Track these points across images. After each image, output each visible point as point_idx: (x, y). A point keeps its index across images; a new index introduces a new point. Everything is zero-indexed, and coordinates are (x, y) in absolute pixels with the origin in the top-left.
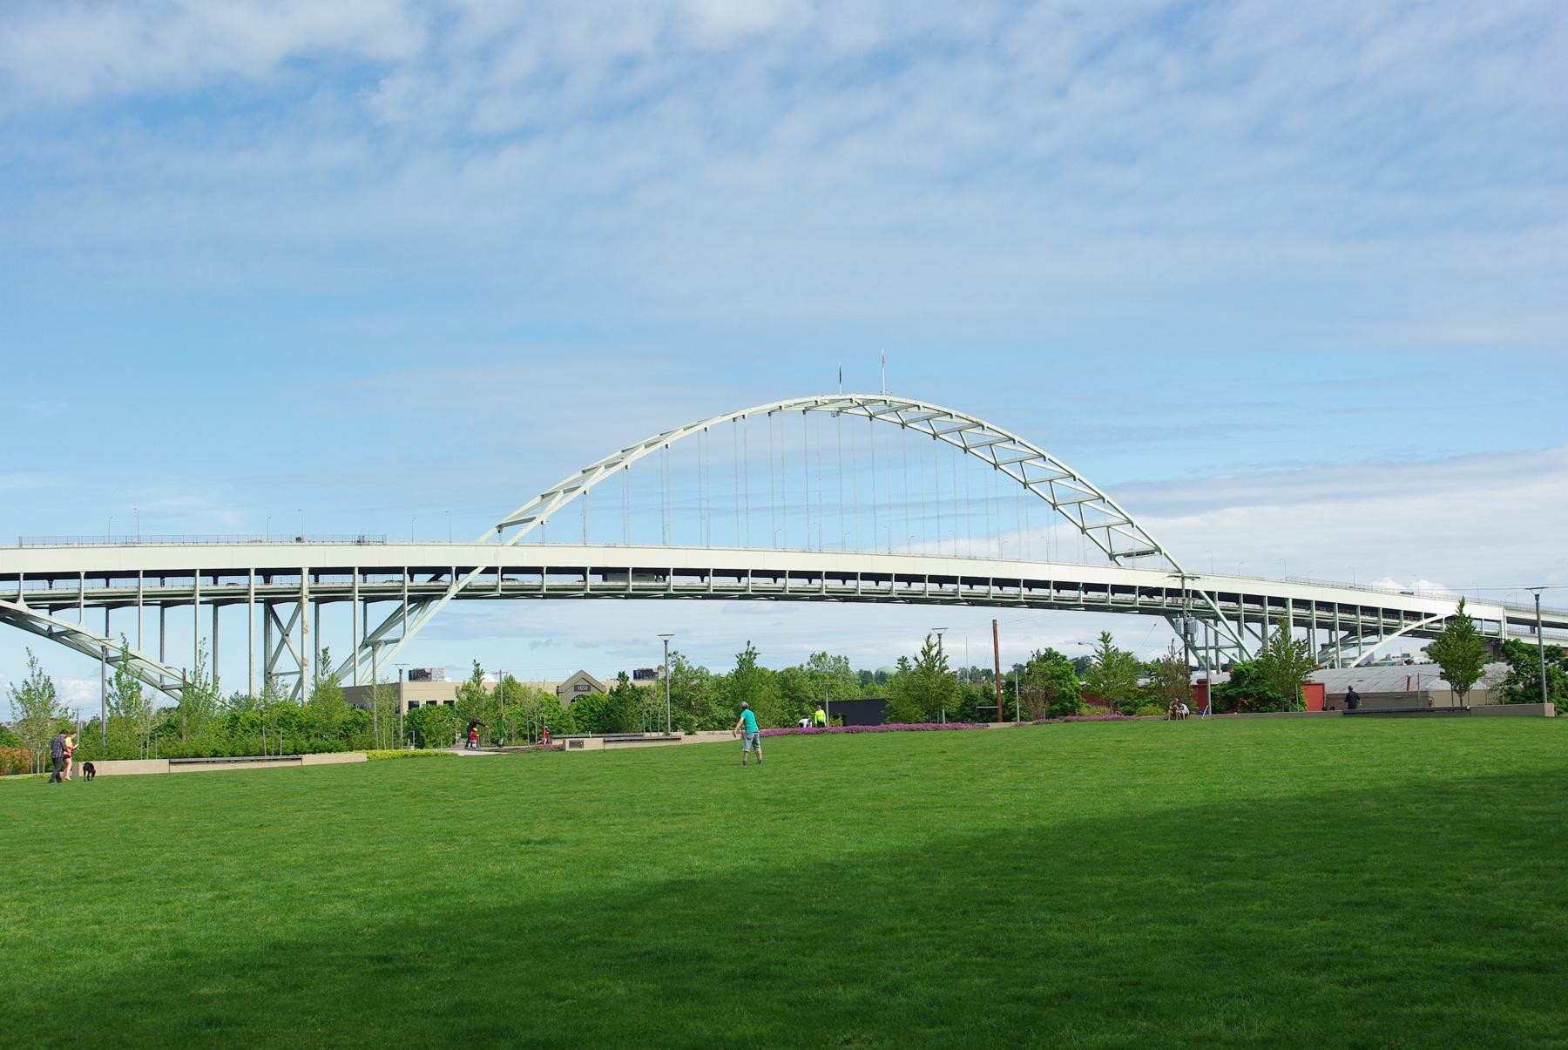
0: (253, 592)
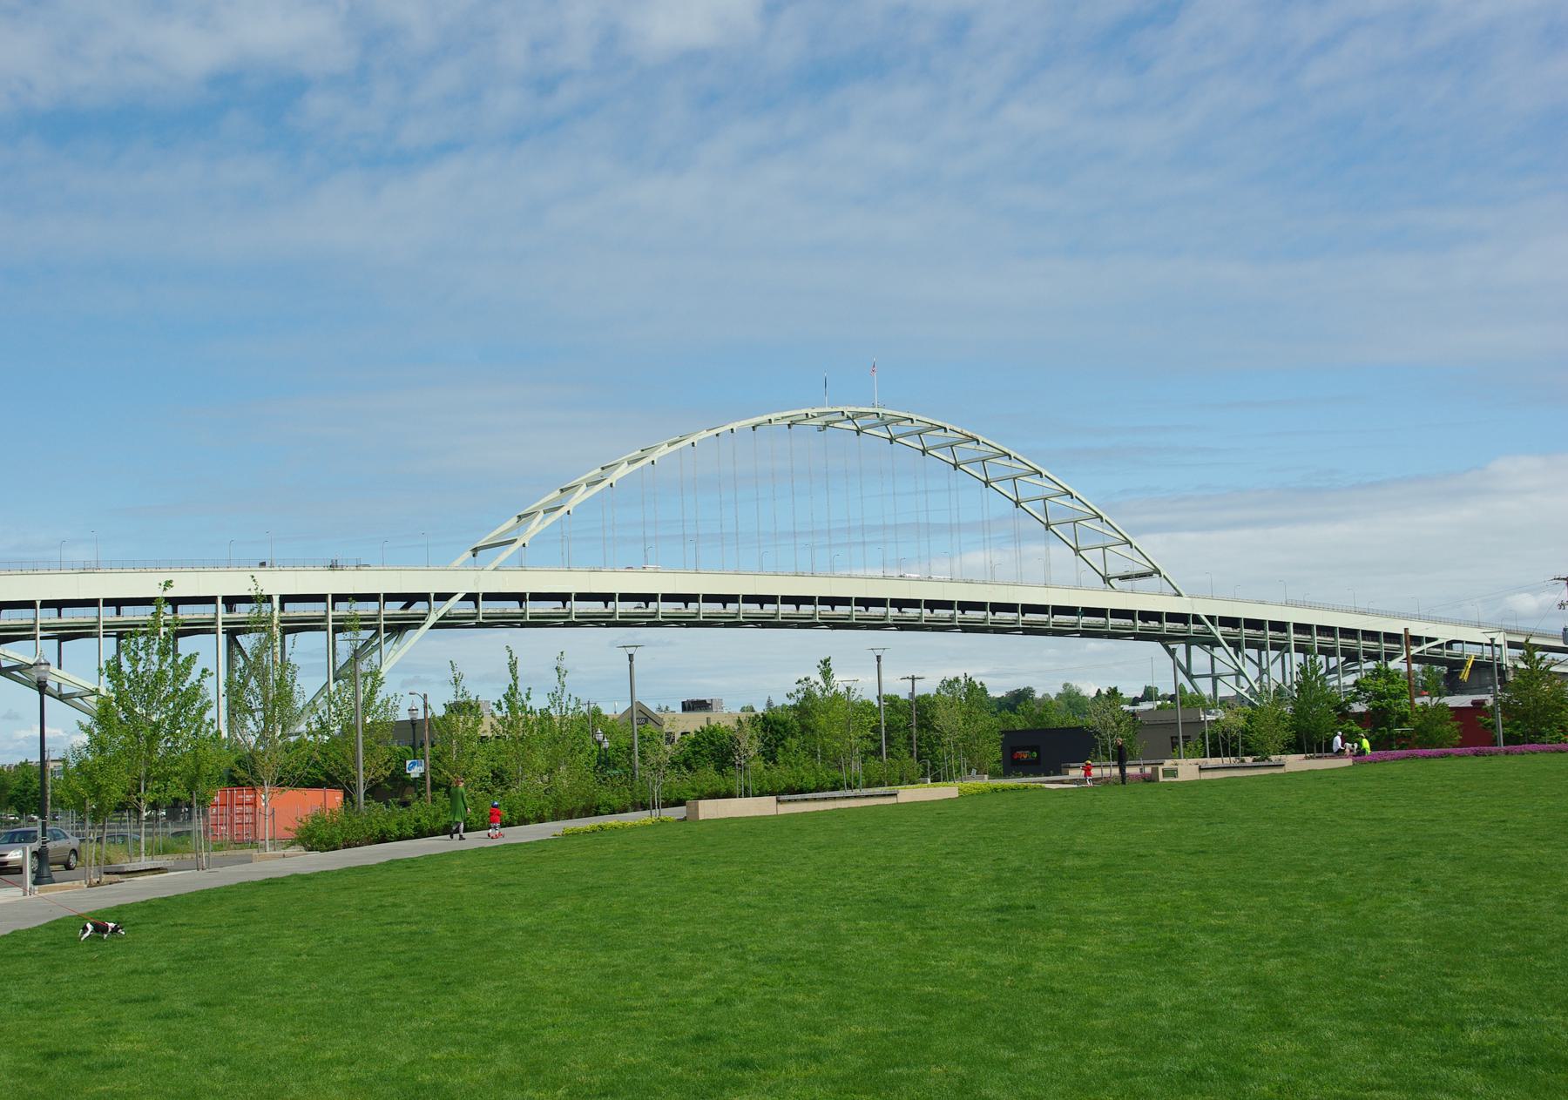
0: (220, 621)
